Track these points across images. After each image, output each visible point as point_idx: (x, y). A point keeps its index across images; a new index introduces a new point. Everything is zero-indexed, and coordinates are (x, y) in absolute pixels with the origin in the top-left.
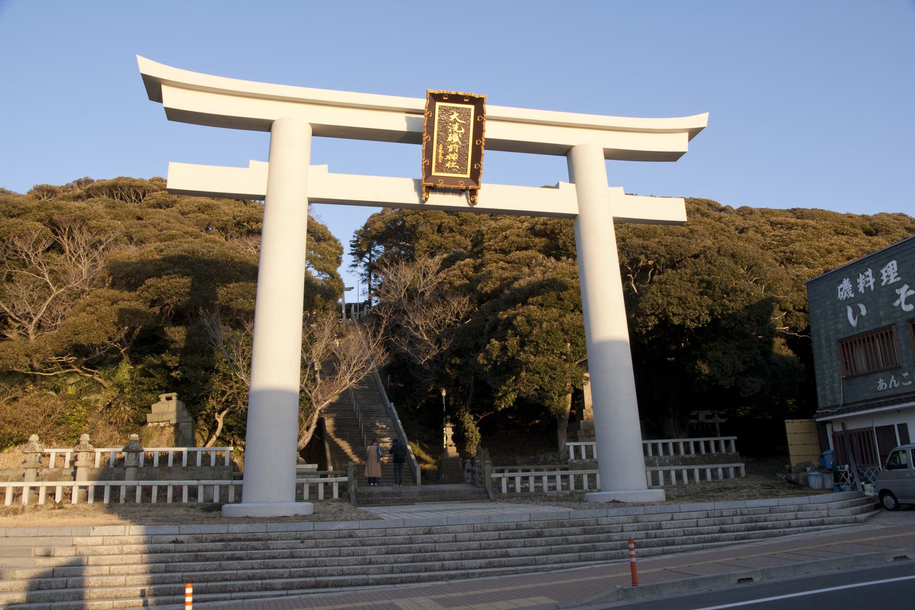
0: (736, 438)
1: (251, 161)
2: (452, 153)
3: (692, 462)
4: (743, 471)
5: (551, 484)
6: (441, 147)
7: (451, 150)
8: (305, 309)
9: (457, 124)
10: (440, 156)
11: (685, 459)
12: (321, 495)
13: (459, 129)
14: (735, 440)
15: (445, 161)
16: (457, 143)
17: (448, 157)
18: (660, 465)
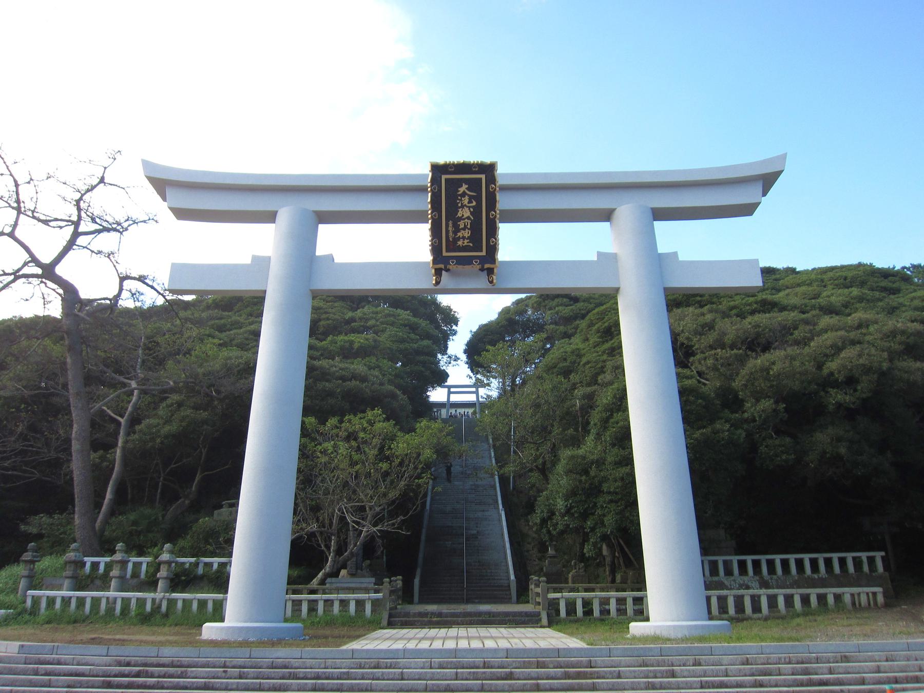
0: (883, 554)
1: (596, 259)
2: (464, 229)
3: (823, 583)
4: (880, 599)
5: (637, 607)
6: (450, 223)
7: (462, 226)
8: (307, 411)
9: (467, 197)
10: (451, 234)
11: (813, 579)
12: (732, 610)
13: (470, 202)
14: (882, 557)
15: (456, 240)
16: (468, 218)
17: (460, 234)
18: (779, 587)
